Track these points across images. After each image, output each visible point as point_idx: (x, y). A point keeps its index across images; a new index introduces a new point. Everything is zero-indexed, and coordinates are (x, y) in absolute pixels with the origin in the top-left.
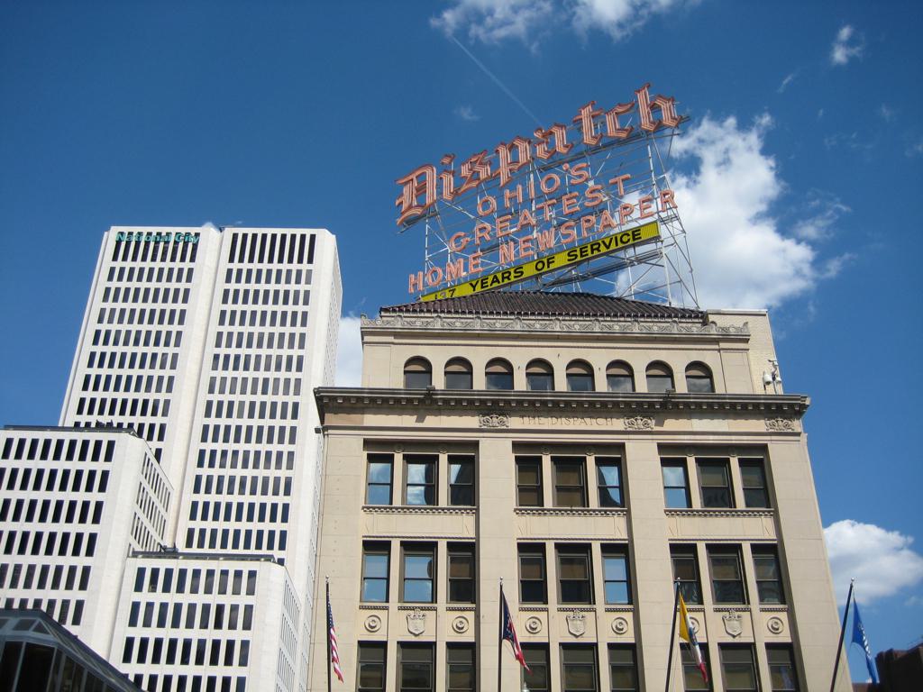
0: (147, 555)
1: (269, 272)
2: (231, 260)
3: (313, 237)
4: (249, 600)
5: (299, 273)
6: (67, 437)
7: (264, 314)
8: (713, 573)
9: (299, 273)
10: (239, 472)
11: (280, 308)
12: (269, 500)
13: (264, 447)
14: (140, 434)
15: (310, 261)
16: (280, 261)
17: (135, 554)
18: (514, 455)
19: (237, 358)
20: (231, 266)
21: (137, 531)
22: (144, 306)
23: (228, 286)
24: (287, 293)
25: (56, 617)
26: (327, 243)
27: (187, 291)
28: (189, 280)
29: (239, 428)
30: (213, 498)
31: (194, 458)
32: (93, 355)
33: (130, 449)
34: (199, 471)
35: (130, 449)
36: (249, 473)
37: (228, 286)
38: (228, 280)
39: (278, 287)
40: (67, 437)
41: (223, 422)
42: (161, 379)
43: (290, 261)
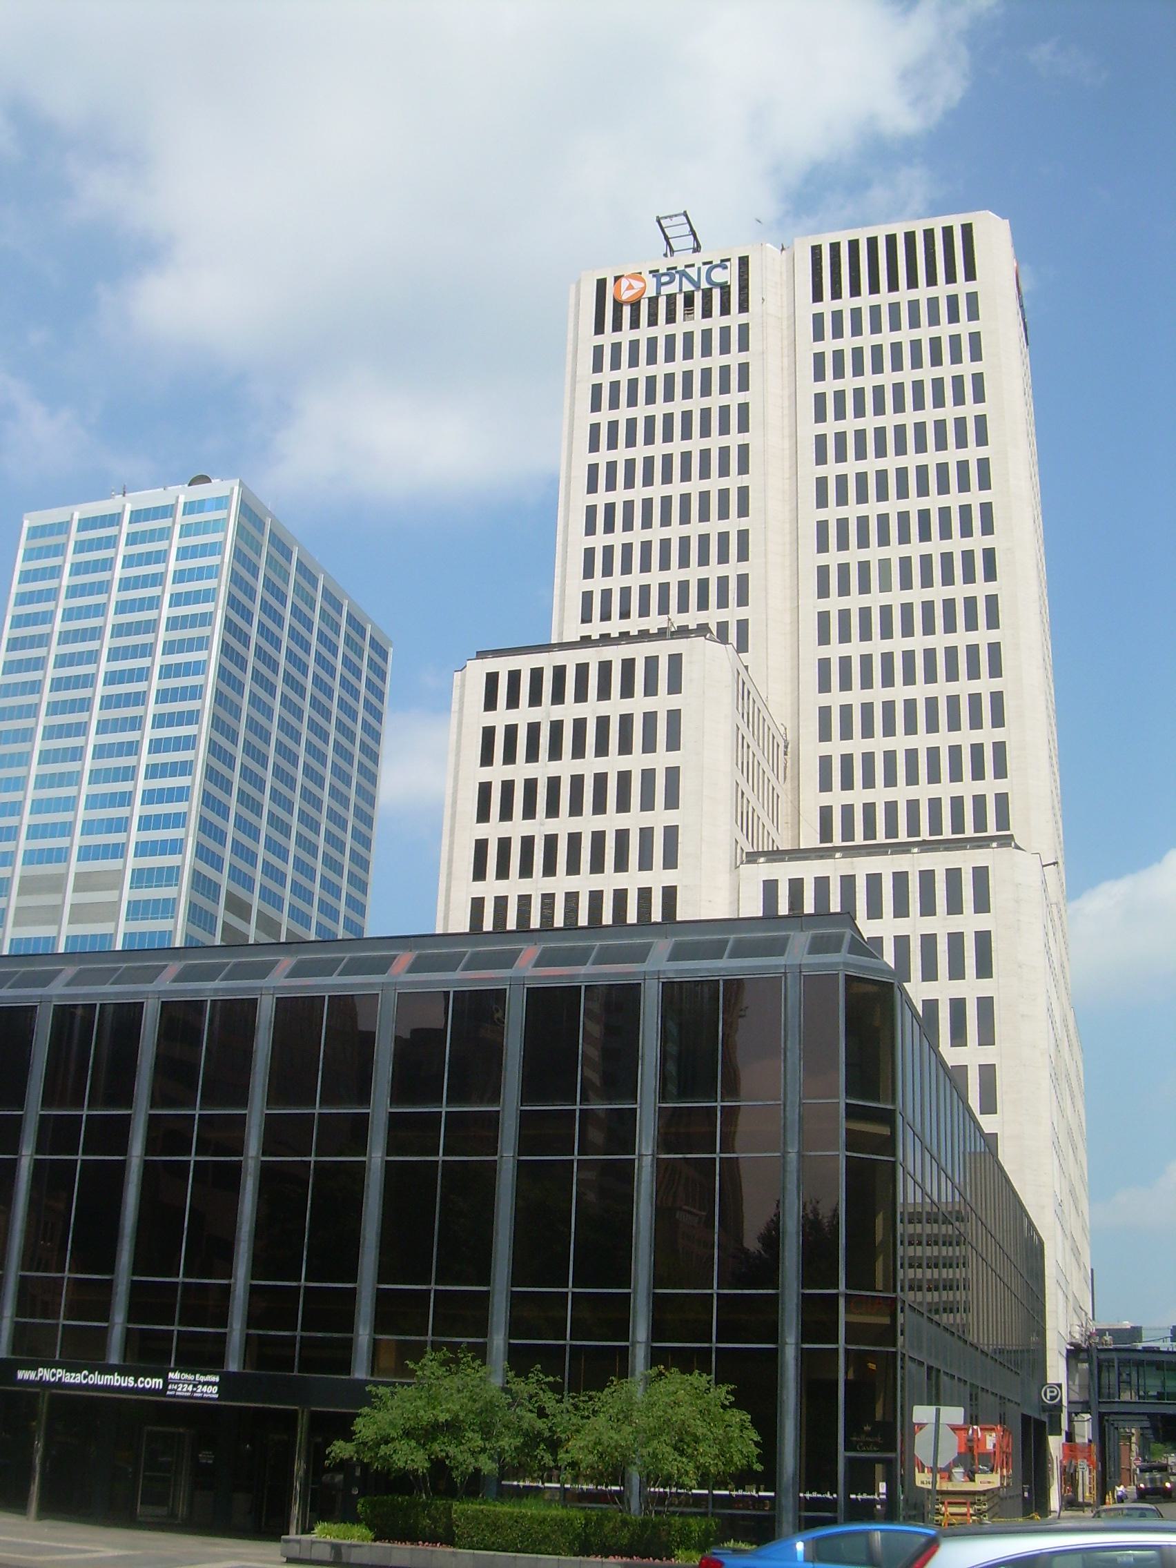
0: (776, 855)
1: (856, 313)
2: (817, 296)
3: (967, 230)
4: (982, 922)
5: (953, 301)
6: (570, 659)
7: (859, 393)
8: (900, 1523)
9: (953, 301)
10: (920, 691)
11: (927, 373)
12: (966, 737)
13: (940, 641)
14: (722, 636)
15: (971, 275)
16: (874, 288)
17: (752, 858)
18: (209, 999)
19: (862, 478)
20: (818, 308)
21: (745, 820)
22: (631, 413)
23: (819, 347)
24: (935, 343)
25: (835, 906)
26: (994, 238)
27: (744, 368)
28: (744, 346)
29: (886, 611)
30: (857, 746)
31: (811, 676)
32: (591, 511)
33: (706, 662)
34: (825, 700)
35: (706, 662)
36: (920, 691)
37: (819, 347)
38: (818, 335)
39: (916, 334)
40: (570, 659)
41: (855, 602)
42: (724, 537)
43: (836, 294)
